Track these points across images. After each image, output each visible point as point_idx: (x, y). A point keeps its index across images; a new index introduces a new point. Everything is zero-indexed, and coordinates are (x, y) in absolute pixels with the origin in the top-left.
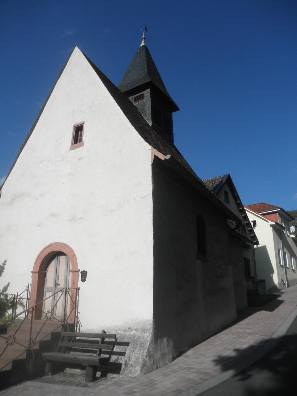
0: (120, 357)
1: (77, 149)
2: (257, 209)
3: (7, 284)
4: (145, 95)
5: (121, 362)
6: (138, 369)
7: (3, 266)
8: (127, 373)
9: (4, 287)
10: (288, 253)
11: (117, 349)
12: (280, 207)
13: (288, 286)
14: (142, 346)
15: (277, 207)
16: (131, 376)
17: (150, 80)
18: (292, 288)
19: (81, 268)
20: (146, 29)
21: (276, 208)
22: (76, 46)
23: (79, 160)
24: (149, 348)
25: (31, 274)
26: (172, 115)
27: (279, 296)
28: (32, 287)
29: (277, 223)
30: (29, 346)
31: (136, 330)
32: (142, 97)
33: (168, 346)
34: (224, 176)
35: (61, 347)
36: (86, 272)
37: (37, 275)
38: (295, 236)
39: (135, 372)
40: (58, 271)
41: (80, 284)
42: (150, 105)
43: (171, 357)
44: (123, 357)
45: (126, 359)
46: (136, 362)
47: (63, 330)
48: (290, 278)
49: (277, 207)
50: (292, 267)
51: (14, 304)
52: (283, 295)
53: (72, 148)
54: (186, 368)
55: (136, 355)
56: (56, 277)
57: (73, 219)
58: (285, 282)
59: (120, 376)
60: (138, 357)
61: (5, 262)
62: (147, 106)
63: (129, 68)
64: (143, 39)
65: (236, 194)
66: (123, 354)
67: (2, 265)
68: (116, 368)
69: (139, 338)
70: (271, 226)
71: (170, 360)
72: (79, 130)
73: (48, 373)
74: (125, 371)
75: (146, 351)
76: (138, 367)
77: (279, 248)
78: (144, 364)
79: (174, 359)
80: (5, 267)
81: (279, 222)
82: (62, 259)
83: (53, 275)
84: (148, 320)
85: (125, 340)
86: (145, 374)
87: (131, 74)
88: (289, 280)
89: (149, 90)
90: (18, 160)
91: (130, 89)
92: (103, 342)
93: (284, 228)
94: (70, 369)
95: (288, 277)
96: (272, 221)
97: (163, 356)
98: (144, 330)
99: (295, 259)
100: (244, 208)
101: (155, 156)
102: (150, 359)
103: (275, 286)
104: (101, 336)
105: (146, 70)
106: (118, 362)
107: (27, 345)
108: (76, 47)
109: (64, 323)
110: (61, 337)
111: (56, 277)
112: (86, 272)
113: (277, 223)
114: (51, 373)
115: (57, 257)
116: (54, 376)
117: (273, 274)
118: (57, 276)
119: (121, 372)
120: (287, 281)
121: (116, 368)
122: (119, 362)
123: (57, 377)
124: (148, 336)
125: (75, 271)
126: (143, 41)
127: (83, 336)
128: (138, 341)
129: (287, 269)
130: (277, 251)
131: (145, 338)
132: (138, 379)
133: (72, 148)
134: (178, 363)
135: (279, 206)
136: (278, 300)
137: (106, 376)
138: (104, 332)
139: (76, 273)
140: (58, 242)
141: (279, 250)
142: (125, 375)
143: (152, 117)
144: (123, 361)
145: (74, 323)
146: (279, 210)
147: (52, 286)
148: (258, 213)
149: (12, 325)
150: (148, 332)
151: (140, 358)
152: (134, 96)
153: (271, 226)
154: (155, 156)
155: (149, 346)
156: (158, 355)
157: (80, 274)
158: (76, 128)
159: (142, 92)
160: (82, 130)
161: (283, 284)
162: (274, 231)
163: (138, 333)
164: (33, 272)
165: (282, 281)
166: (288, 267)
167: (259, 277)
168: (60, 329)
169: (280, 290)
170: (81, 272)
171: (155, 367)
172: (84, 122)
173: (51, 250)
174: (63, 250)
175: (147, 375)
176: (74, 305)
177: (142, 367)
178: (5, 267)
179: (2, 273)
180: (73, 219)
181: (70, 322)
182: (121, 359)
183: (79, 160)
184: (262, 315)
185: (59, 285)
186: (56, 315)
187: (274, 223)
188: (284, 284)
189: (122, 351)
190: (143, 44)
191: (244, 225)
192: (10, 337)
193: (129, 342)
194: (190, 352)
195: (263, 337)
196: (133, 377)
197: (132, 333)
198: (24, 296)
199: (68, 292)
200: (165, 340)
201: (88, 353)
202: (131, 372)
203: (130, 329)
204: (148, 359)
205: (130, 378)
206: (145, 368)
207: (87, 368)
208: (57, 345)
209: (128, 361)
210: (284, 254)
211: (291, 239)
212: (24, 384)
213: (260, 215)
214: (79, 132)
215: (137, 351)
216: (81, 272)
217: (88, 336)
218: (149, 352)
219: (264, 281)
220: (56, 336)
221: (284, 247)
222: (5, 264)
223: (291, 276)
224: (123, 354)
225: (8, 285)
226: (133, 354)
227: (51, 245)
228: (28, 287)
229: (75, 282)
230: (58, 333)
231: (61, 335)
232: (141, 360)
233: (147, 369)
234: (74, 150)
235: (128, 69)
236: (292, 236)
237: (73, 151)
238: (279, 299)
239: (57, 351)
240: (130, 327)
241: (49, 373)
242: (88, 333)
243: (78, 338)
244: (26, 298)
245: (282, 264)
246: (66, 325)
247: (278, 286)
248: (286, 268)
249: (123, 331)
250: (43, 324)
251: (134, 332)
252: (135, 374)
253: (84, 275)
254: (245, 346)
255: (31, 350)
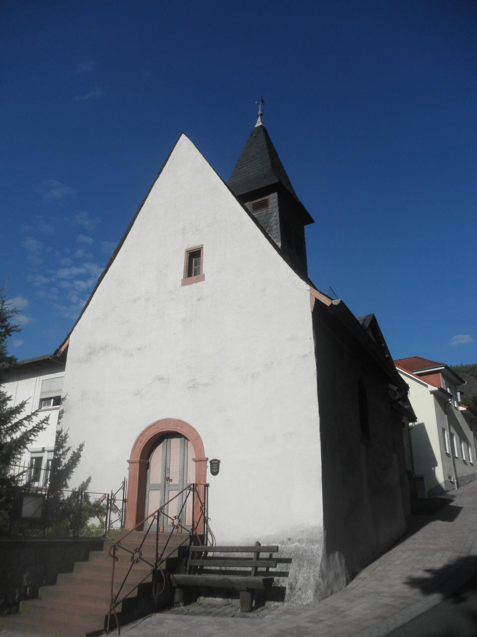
0: (281, 579)
1: (194, 285)
2: (410, 368)
3: (87, 478)
4: (271, 202)
5: (283, 585)
6: (310, 593)
7: (78, 452)
8: (295, 600)
9: (82, 483)
10: (456, 434)
11: (280, 567)
12: (444, 364)
13: (458, 487)
14: (311, 562)
15: (440, 364)
16: (302, 604)
17: (277, 181)
18: (464, 489)
19: (210, 455)
20: (263, 101)
21: (439, 365)
22: (182, 133)
23: (199, 300)
24: (321, 565)
25: (128, 465)
26: (304, 230)
27: (451, 501)
28: (129, 484)
29: (441, 389)
30: (156, 564)
31: (299, 541)
32: (265, 204)
33: (341, 563)
34: (367, 317)
35: (192, 566)
36: (219, 462)
37: (137, 466)
38: (467, 409)
39: (307, 597)
40: (168, 460)
41: (210, 478)
42: (278, 218)
43: (345, 579)
44: (285, 579)
45: (291, 580)
46: (306, 585)
47: (192, 544)
48: (460, 474)
49: (440, 364)
50: (463, 457)
51: (98, 510)
52: (455, 499)
53: (184, 283)
54: (372, 592)
55: (305, 575)
56: (166, 470)
57: (194, 385)
58: (453, 479)
59: (286, 604)
60: (309, 578)
61: (81, 446)
62: (273, 219)
63: (240, 158)
64: (260, 117)
65: (383, 345)
66: (285, 574)
67: (76, 452)
68: (279, 594)
69: (306, 552)
70: (432, 392)
71: (345, 583)
72: (194, 256)
73: (179, 602)
74: (291, 598)
75: (318, 569)
76: (311, 591)
77: (444, 427)
78: (317, 589)
79: (348, 581)
80: (81, 454)
81: (443, 385)
82: (175, 442)
83: (160, 465)
84: (316, 527)
85: (285, 556)
86: (320, 601)
87: (245, 168)
88: (458, 476)
89: (275, 195)
90: (94, 296)
91: (247, 191)
92: (258, 558)
93: (450, 396)
94: (206, 598)
95: (458, 474)
96: (433, 385)
97: (337, 576)
98: (311, 541)
99: (466, 444)
100: (397, 368)
101: (316, 299)
102: (323, 580)
103: (439, 486)
104: (256, 550)
105: (269, 164)
106: (279, 586)
107: (153, 562)
108: (183, 136)
109: (193, 533)
110: (191, 553)
111: (166, 470)
112: (219, 462)
113: (441, 389)
114: (183, 604)
115: (165, 440)
116: (188, 607)
117: (436, 468)
118: (168, 466)
119: (286, 598)
120: (457, 479)
121: (279, 594)
122: (281, 585)
123: (192, 607)
124: (318, 548)
125: (200, 460)
126: (259, 120)
127: (226, 550)
128: (305, 556)
129: (456, 459)
130: (441, 431)
131: (314, 552)
132: (314, 607)
133: (184, 283)
134: (356, 587)
135: (442, 362)
136: (451, 506)
137: (263, 605)
138: (258, 544)
139: (202, 463)
140: (171, 419)
141: (444, 430)
142: (293, 602)
143: (281, 234)
144: (287, 584)
145: (202, 533)
146: (443, 368)
147: (159, 483)
148: (411, 373)
149: (107, 538)
150: (317, 544)
151: (312, 578)
152: (252, 202)
153: (432, 392)
154: (316, 299)
155: (322, 561)
156: (331, 575)
157: (209, 464)
158: (190, 253)
159: (264, 196)
160: (200, 256)
161: (450, 484)
162: (437, 401)
163: (303, 545)
164: (130, 462)
165: (450, 478)
166: (457, 456)
167: (418, 472)
168: (187, 543)
169: (447, 491)
170: (211, 462)
171: (329, 593)
172: (202, 245)
173: (159, 429)
174: (178, 430)
175: (323, 601)
176: (203, 507)
177: (316, 591)
178: (82, 453)
179: (77, 463)
180: (194, 385)
181: (200, 532)
182: (283, 581)
183: (199, 300)
184: (436, 528)
185: (171, 480)
186: (168, 524)
187: (436, 389)
188: (452, 483)
189: (282, 571)
190: (259, 123)
191: (394, 391)
192: (136, 551)
193: (291, 557)
194: (364, 574)
195: (458, 554)
196: (305, 604)
197: (293, 545)
198: (119, 496)
199: (196, 489)
200: (337, 554)
201: (244, 571)
202: (300, 598)
203: (289, 539)
204: (321, 580)
205: (300, 605)
206: (319, 593)
207: (242, 594)
208: (186, 565)
209: (294, 584)
210: (451, 436)
211: (460, 412)
212: (153, 616)
213: (413, 375)
214: (194, 259)
215: (304, 569)
216: (211, 462)
217: (235, 550)
218: (321, 571)
219: (421, 479)
220: (184, 551)
221: (451, 426)
222: (82, 450)
223: (463, 471)
224: (285, 574)
225: (89, 480)
226: (299, 573)
227: (158, 422)
228: (124, 484)
229: (201, 475)
230: (185, 547)
231: (191, 550)
232: (312, 581)
233: (325, 592)
234: (190, 286)
235: (239, 161)
236: (462, 408)
237: (187, 287)
238: (452, 504)
239: (187, 572)
240: (289, 537)
241: (181, 603)
242: (226, 545)
243: (210, 554)
244: (122, 499)
245: (448, 452)
246: (195, 536)
247: (443, 486)
248: (454, 457)
249: (280, 543)
250: (169, 537)
251: (296, 544)
252: (308, 600)
253: (215, 467)
254: (439, 565)
255: (159, 571)
